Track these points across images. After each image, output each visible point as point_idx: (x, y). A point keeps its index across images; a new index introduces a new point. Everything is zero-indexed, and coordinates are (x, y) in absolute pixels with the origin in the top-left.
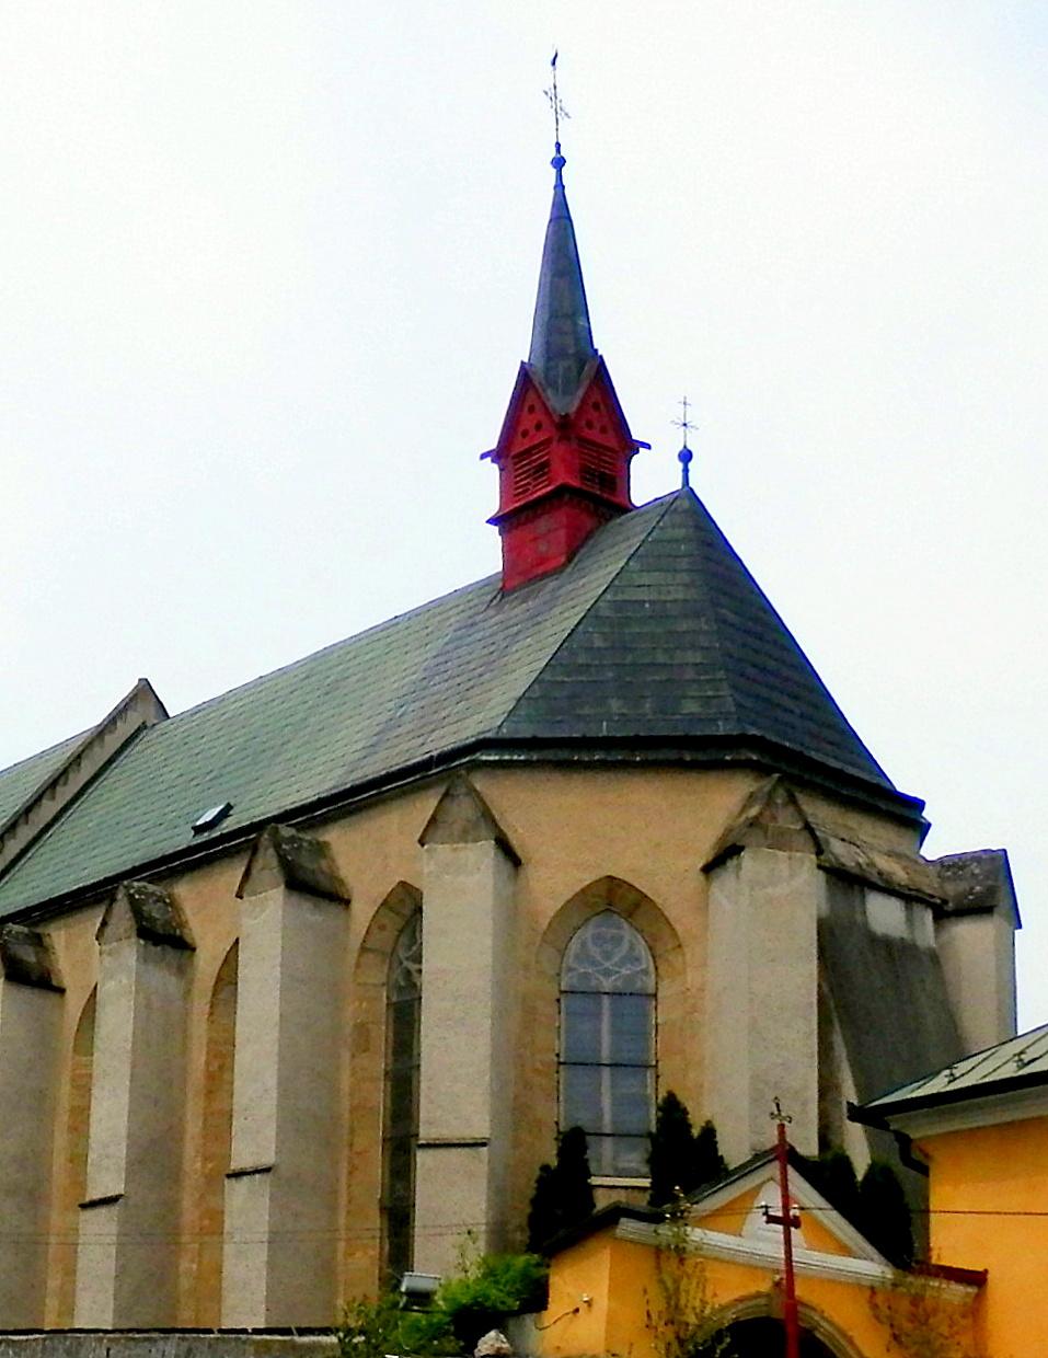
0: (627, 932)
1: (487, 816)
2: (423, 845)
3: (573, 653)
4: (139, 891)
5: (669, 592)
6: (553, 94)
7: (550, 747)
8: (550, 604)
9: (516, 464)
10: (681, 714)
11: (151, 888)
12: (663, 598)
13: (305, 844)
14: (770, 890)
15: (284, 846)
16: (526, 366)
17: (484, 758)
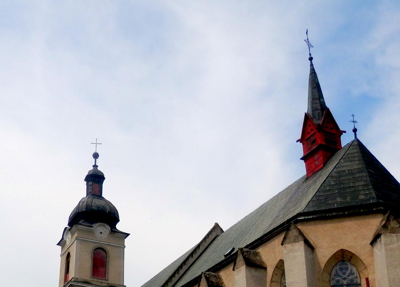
0: (350, 267)
1: (301, 233)
2: (282, 245)
3: (325, 187)
4: (208, 275)
5: (353, 167)
6: (307, 41)
7: (320, 213)
8: (320, 176)
9: (307, 142)
10: (359, 199)
11: (212, 273)
12: (351, 169)
13: (252, 253)
14: (391, 246)
15: (245, 254)
16: (307, 114)
17: (300, 219)
